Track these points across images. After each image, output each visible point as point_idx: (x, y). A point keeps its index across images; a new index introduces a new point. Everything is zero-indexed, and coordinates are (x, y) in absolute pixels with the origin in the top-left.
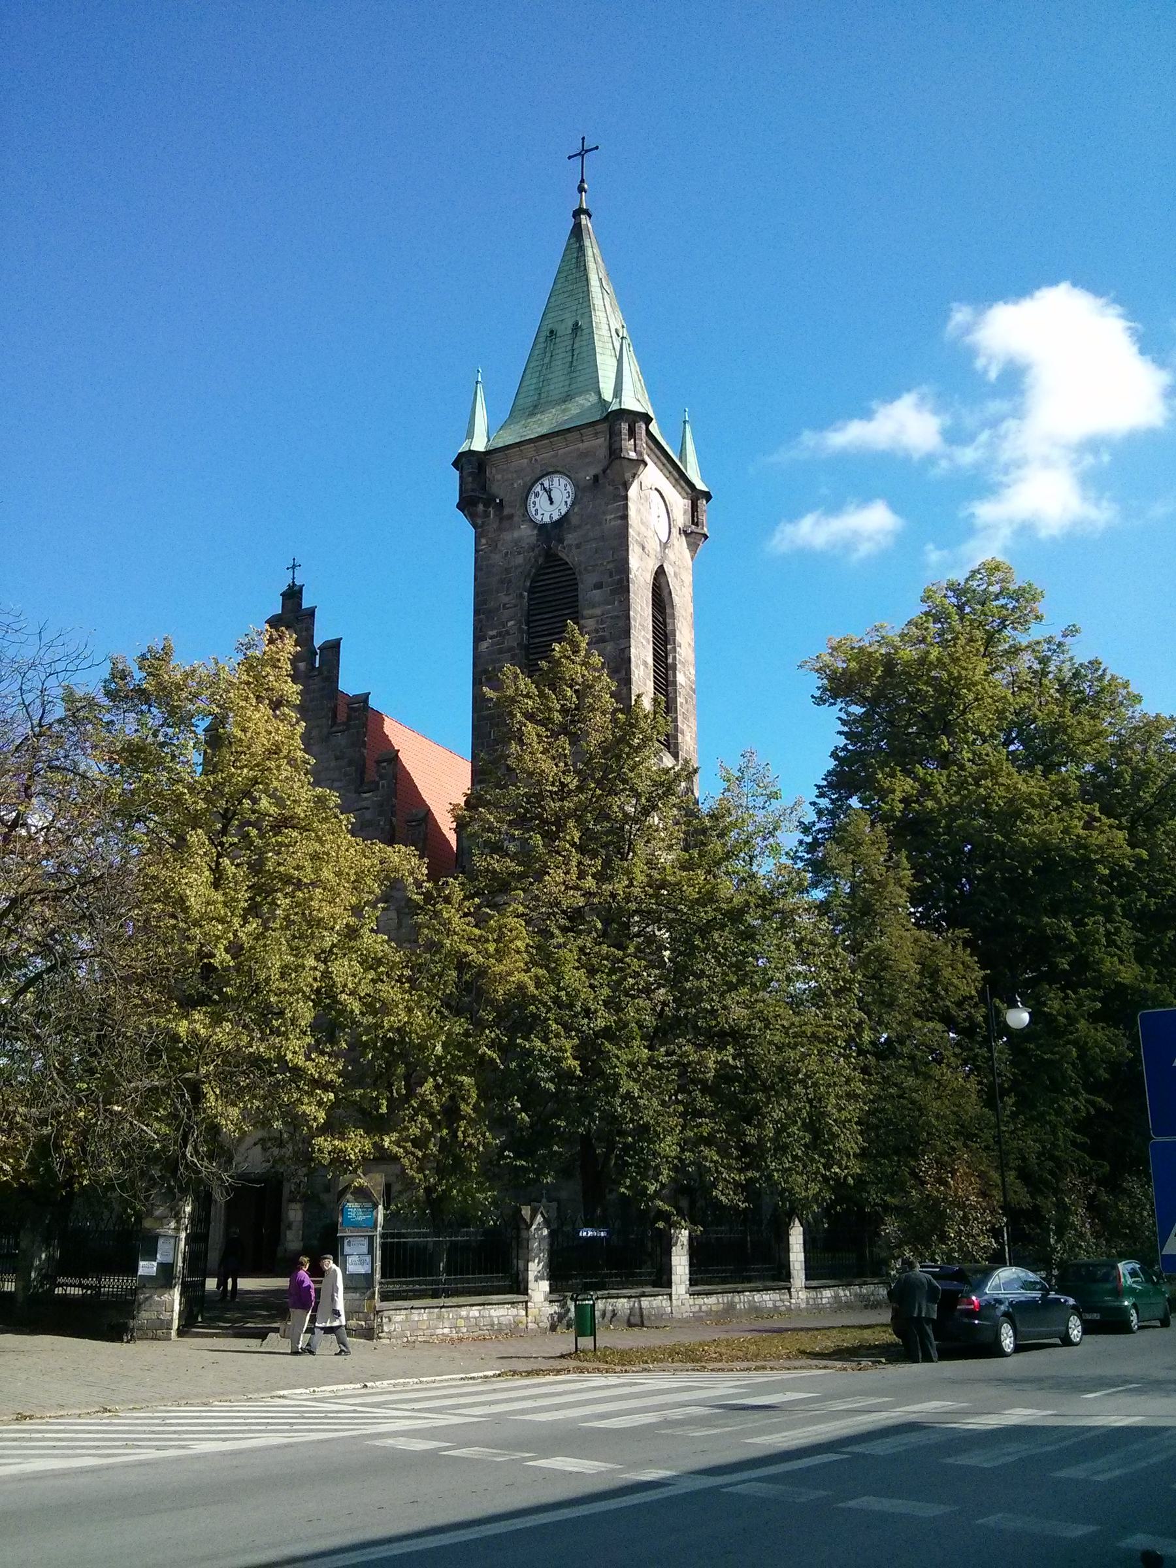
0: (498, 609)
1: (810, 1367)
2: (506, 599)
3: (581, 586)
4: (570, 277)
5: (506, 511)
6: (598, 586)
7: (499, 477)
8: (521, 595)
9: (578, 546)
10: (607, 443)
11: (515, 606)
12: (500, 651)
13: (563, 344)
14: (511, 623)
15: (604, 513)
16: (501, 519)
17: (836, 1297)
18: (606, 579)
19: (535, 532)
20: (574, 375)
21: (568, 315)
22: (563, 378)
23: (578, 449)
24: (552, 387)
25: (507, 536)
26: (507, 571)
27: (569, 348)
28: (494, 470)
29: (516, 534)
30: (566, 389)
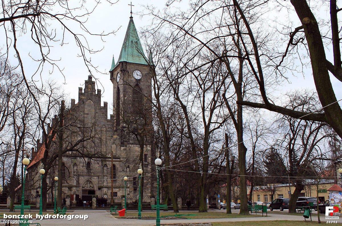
2: (130, 91)
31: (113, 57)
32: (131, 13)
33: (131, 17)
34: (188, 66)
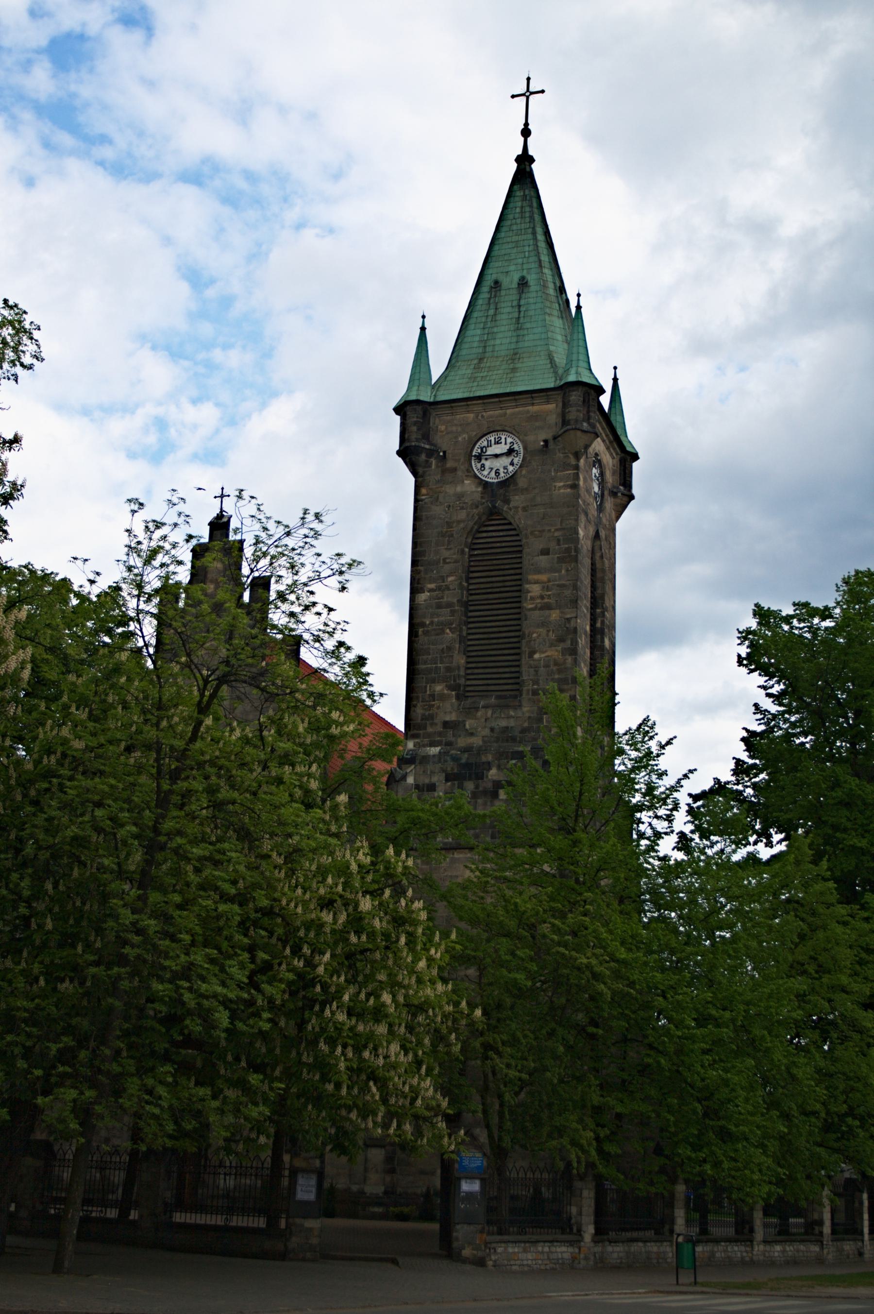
0: (438, 562)
1: (756, 1302)
2: (446, 554)
3: (526, 550)
4: (514, 227)
5: (450, 464)
6: (545, 552)
7: (443, 428)
8: (463, 552)
9: (525, 509)
10: (559, 410)
11: (456, 562)
12: (439, 606)
13: (508, 298)
14: (450, 579)
15: (554, 479)
16: (444, 471)
17: (784, 1251)
18: (553, 545)
19: (480, 489)
20: (521, 332)
21: (512, 268)
22: (510, 334)
23: (528, 412)
24: (498, 342)
25: (450, 490)
26: (449, 524)
27: (515, 303)
28: (437, 421)
29: (459, 489)
30: (513, 346)
31: (423, 329)
32: (526, 132)
33: (525, 160)
34: (140, 539)
